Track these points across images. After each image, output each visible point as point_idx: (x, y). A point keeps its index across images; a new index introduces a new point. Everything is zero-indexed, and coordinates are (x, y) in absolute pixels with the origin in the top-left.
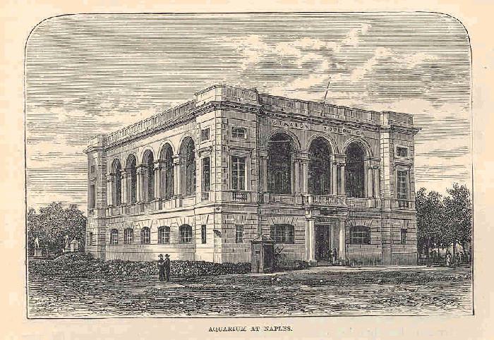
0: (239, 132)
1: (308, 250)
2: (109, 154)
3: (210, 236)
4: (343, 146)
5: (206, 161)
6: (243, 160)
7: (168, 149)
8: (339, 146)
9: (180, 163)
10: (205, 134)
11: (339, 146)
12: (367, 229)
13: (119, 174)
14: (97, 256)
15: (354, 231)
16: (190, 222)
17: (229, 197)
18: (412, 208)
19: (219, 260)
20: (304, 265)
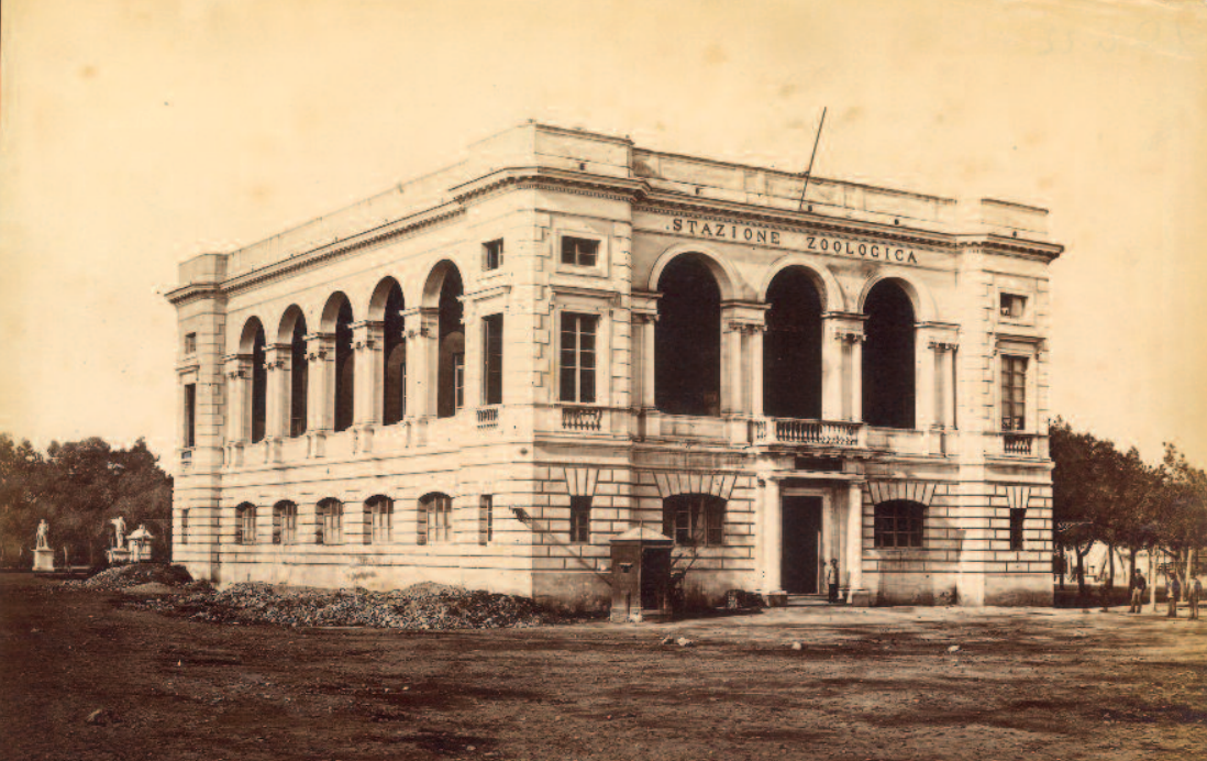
0: (579, 251)
1: (762, 571)
2: (236, 302)
3: (504, 523)
4: (857, 287)
5: (494, 324)
6: (590, 322)
7: (294, 318)
8: (843, 292)
9: (279, 364)
10: (494, 251)
11: (843, 292)
12: (633, 522)
13: (258, 358)
14: (198, 570)
15: (899, 522)
16: (292, 495)
17: (553, 420)
18: (1040, 450)
19: (523, 586)
20: (751, 603)
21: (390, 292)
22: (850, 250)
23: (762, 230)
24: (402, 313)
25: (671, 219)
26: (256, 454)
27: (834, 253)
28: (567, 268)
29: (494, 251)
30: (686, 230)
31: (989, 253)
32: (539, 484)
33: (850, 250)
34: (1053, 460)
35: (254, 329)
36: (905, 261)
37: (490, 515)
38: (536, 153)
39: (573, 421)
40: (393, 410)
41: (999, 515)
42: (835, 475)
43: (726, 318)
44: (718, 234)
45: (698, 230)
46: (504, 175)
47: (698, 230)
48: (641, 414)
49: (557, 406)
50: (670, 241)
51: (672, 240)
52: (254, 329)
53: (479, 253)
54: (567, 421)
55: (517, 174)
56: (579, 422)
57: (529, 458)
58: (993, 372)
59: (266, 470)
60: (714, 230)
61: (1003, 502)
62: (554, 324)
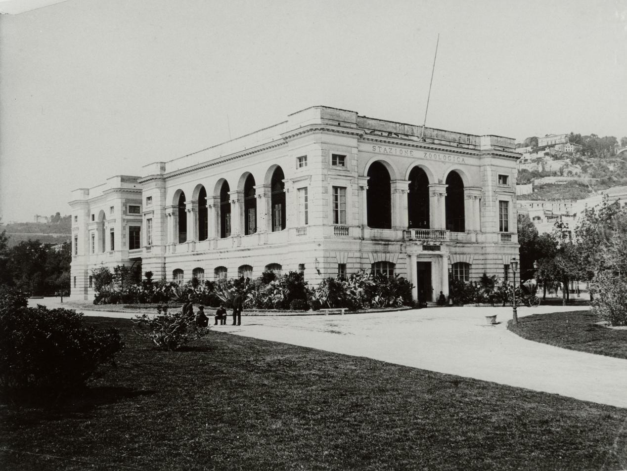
0: (339, 159)
8: (437, 176)
21: (249, 181)
22: (440, 158)
23: (406, 150)
24: (229, 193)
25: (372, 145)
26: (182, 248)
27: (434, 159)
28: (334, 167)
29: (302, 159)
30: (377, 150)
31: (494, 158)
32: (326, 259)
33: (440, 158)
34: (520, 244)
35: (181, 197)
36: (461, 162)
37: (514, 279)
38: (321, 118)
39: (343, 233)
40: (225, 231)
41: (495, 270)
42: (437, 252)
43: (393, 187)
44: (390, 152)
45: (382, 150)
46: (309, 128)
47: (382, 150)
48: (362, 227)
49: (332, 226)
50: (372, 153)
51: (371, 155)
52: (181, 197)
53: (109, 209)
54: (336, 233)
55: (314, 128)
56: (340, 233)
57: (322, 247)
58: (527, 203)
59: (194, 255)
60: (388, 150)
61: (500, 262)
62: (331, 191)
